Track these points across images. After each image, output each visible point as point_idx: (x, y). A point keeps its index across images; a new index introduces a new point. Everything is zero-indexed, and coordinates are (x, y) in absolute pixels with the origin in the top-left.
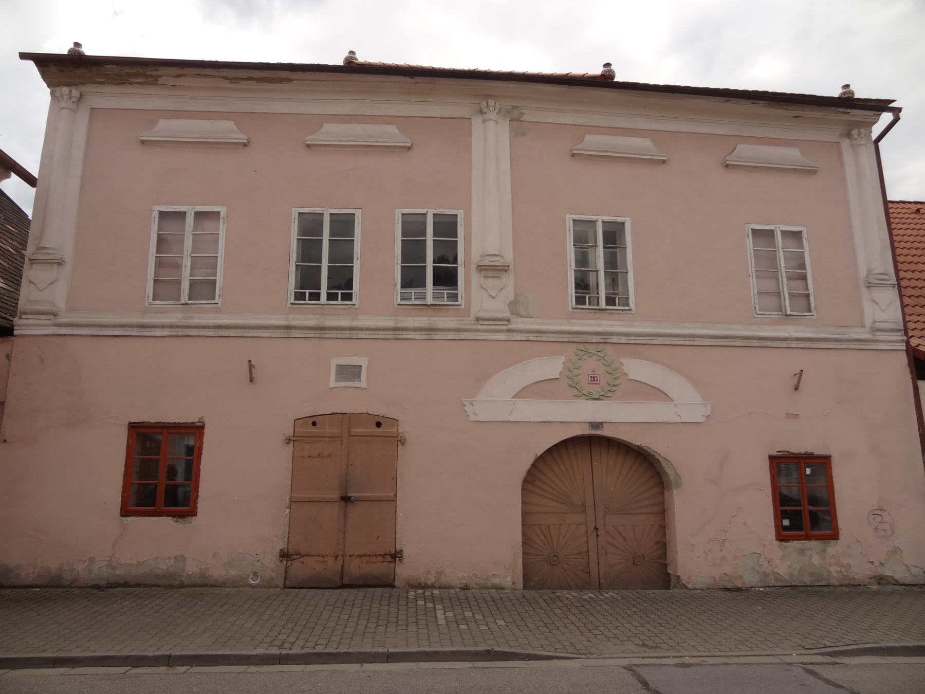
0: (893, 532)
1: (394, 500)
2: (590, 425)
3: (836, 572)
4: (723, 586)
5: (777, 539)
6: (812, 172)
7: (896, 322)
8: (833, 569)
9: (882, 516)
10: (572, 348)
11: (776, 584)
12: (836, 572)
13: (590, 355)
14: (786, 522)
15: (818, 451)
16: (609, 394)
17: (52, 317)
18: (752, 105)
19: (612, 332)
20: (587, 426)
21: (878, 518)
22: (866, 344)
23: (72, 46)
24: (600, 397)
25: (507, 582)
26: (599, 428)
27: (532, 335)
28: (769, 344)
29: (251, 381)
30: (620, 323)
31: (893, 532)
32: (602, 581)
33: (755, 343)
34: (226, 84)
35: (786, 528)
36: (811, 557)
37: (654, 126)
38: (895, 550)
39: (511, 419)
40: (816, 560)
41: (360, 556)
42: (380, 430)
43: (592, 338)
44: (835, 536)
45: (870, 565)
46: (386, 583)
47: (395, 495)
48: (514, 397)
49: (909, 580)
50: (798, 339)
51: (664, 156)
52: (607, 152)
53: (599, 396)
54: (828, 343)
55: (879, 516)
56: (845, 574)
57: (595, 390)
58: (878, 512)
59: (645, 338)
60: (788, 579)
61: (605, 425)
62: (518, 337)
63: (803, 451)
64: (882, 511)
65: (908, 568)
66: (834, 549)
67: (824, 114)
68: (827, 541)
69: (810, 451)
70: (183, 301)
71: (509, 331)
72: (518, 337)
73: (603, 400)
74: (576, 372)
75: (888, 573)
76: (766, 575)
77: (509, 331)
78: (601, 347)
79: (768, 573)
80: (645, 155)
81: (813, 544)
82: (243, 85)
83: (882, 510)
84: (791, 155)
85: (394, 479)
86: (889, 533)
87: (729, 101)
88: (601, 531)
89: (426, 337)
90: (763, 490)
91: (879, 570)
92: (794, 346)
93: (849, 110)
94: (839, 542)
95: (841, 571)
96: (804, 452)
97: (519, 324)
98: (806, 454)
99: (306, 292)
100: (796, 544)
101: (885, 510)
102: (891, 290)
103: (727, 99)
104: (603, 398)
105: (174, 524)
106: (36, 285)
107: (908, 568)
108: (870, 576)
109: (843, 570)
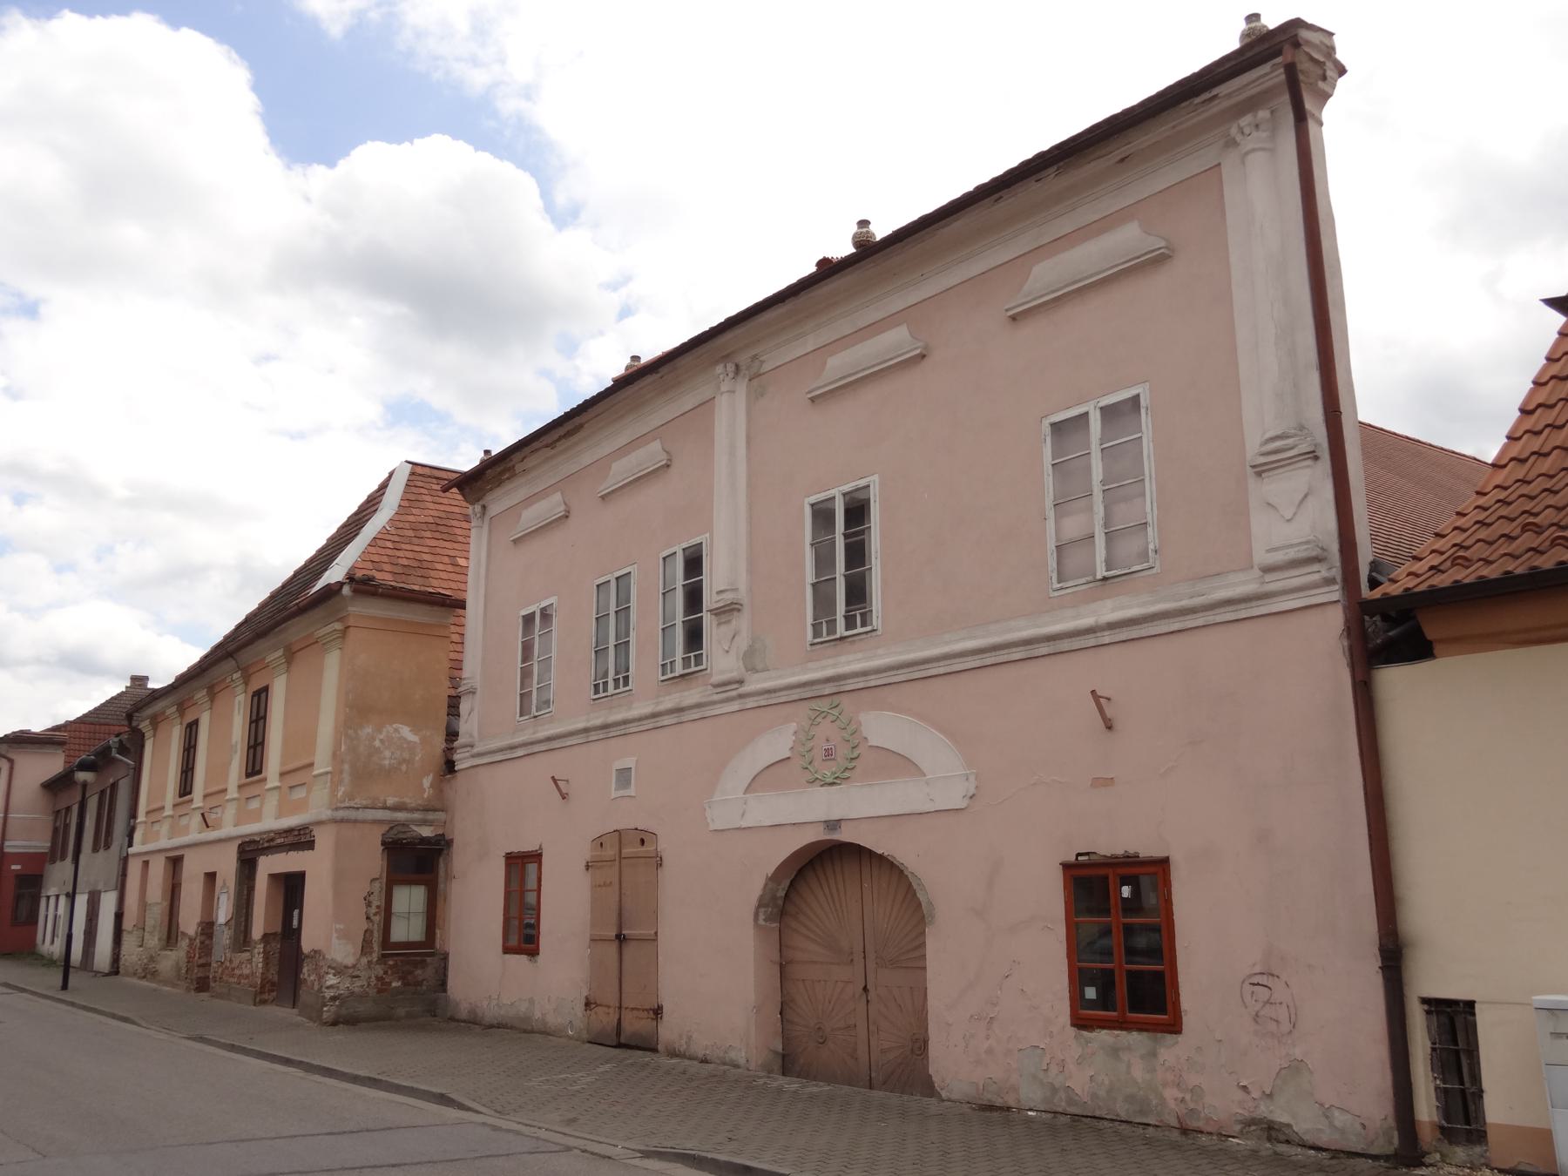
0: (1294, 1026)
1: (654, 939)
2: (825, 826)
3: (1176, 1099)
4: (989, 1101)
5: (1073, 1025)
6: (1158, 260)
7: (1307, 542)
8: (1170, 1094)
9: (1270, 988)
10: (804, 710)
11: (1068, 1109)
12: (1176, 1099)
13: (823, 715)
14: (1091, 993)
15: (1148, 850)
16: (846, 774)
17: (469, 749)
18: (1039, 184)
19: (1195, 608)
20: (821, 827)
21: (1262, 993)
22: (1249, 605)
23: (482, 455)
24: (835, 781)
25: (739, 1056)
26: (836, 829)
27: (762, 697)
28: (1065, 645)
29: (1109, 728)
30: (860, 655)
31: (1294, 1026)
32: (873, 1075)
33: (1044, 649)
34: (548, 452)
35: (1091, 1004)
36: (1129, 1066)
37: (897, 303)
38: (1296, 1068)
39: (744, 824)
40: (1138, 1073)
41: (633, 1009)
42: (644, 849)
43: (825, 688)
44: (1174, 1027)
45: (1240, 1095)
46: (647, 1045)
47: (656, 933)
48: (747, 791)
49: (1324, 1139)
50: (1112, 626)
51: (916, 348)
52: (844, 377)
53: (836, 778)
54: (1172, 620)
55: (1266, 989)
56: (1192, 1106)
57: (827, 771)
58: (1263, 979)
59: (941, 664)
60: (1089, 1102)
61: (843, 824)
62: (751, 703)
63: (1120, 851)
64: (1270, 978)
65: (1326, 1112)
66: (1172, 1051)
67: (1172, 125)
68: (1159, 1035)
69: (1132, 851)
70: (1099, 576)
71: (741, 696)
72: (751, 703)
73: (840, 784)
74: (810, 744)
75: (1281, 1117)
76: (1054, 1090)
77: (741, 696)
78: (836, 699)
79: (1057, 1086)
80: (891, 359)
81: (1134, 1038)
82: (561, 446)
83: (1273, 975)
84: (1128, 239)
85: (656, 912)
86: (1286, 1027)
87: (1001, 197)
88: (872, 995)
89: (674, 721)
90: (1052, 929)
91: (1262, 1108)
92: (1107, 640)
93: (1215, 91)
94: (1180, 1038)
95: (1183, 1100)
96: (1122, 852)
97: (755, 683)
98: (1128, 857)
99: (690, 657)
100: (1104, 1036)
101: (1278, 977)
102: (1308, 466)
103: (997, 196)
104: (839, 782)
105: (527, 962)
106: (1278, 511)
107: (1326, 1112)
108: (1240, 1118)
109: (1188, 1097)
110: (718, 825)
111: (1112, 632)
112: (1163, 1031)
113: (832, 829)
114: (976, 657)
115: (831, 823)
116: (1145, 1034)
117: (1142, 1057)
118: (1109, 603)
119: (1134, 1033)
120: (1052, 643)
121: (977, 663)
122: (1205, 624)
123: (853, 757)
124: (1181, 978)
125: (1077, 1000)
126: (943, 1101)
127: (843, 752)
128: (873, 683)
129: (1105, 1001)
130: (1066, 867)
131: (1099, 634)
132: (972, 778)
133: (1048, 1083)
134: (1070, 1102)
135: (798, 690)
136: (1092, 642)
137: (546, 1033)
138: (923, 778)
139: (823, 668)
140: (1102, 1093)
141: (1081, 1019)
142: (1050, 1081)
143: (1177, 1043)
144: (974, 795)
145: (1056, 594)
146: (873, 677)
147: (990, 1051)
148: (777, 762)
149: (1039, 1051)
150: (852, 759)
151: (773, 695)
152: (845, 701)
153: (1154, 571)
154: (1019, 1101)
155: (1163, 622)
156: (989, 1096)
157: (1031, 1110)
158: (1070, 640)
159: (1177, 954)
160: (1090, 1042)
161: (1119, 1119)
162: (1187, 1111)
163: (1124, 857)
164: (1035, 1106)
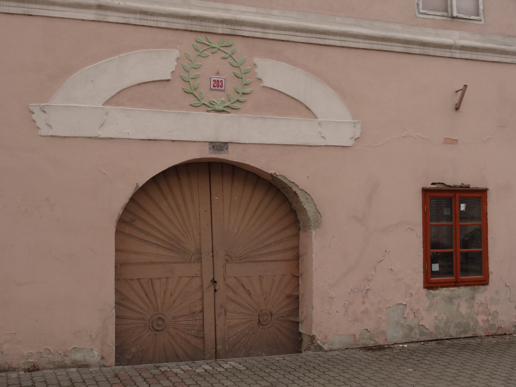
5: (425, 287)
8: (480, 318)
13: (214, 50)
15: (475, 184)
16: (237, 105)
20: (207, 147)
24: (225, 109)
28: (431, 51)
32: (219, 347)
33: (416, 50)
35: (435, 273)
39: (102, 134)
48: (107, 102)
50: (463, 48)
56: (492, 323)
59: (338, 38)
61: (230, 147)
63: (459, 184)
68: (476, 287)
69: (466, 184)
73: (229, 113)
74: (194, 73)
76: (411, 329)
78: (229, 41)
79: (413, 327)
81: (462, 290)
88: (220, 285)
90: (413, 230)
92: (458, 56)
94: (488, 287)
100: (444, 292)
104: (229, 111)
109: (490, 318)
110: (41, 134)
111: (461, 52)
112: (479, 285)
113: (217, 150)
114: (367, 41)
115: (217, 144)
116: (469, 287)
117: (466, 301)
118: (457, 34)
119: (463, 287)
120: (421, 47)
121: (367, 46)
122: (512, 62)
123: (245, 92)
124: (490, 255)
125: (428, 273)
126: (326, 352)
127: (230, 86)
128: (271, 36)
129: (446, 271)
130: (425, 191)
131: (452, 51)
132: (359, 126)
133: (407, 325)
134: (422, 334)
135: (184, 21)
136: (448, 54)
137: (389, 347)
138: (317, 120)
139: (215, 9)
140: (442, 325)
141: (430, 283)
142: (408, 323)
143: (486, 290)
144: (358, 138)
145: (421, 16)
146: (271, 31)
147: (365, 312)
148: (154, 81)
149: (401, 306)
150: (243, 94)
151: (149, 17)
152: (238, 45)
153: (481, 23)
154: (386, 340)
155: (489, 54)
156: (364, 341)
157: (386, 345)
158: (434, 49)
159: (488, 242)
160: (435, 297)
161: (452, 337)
162: (489, 326)
163: (460, 187)
164: (399, 341)
